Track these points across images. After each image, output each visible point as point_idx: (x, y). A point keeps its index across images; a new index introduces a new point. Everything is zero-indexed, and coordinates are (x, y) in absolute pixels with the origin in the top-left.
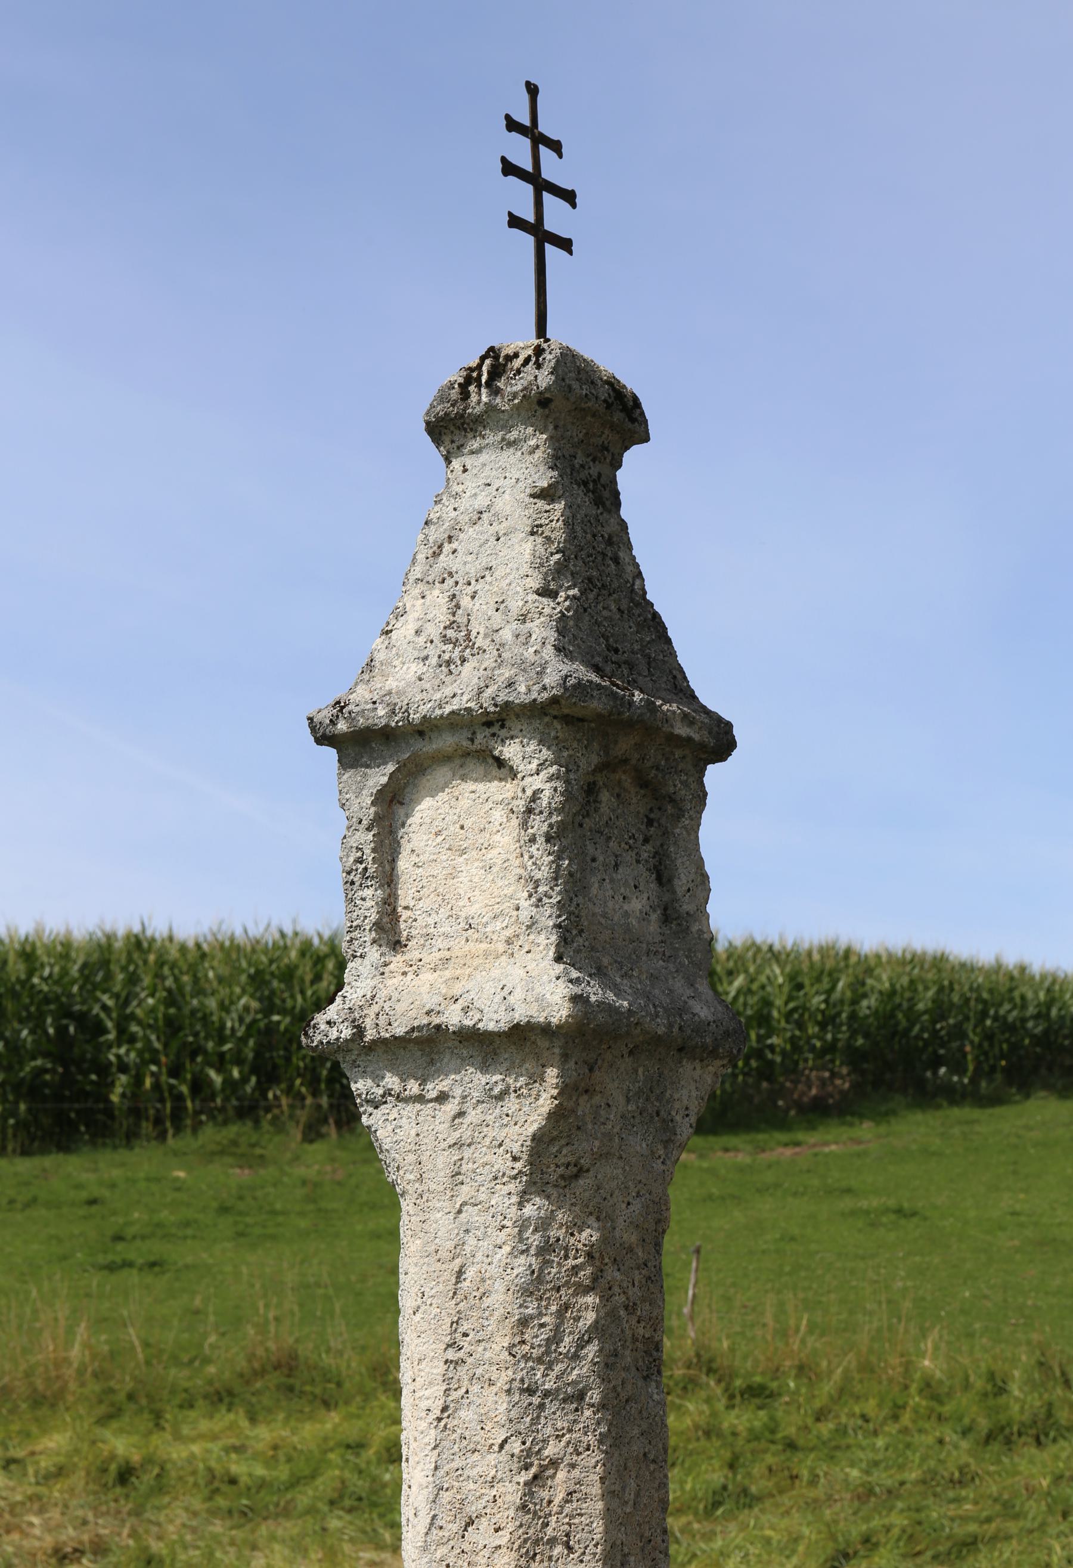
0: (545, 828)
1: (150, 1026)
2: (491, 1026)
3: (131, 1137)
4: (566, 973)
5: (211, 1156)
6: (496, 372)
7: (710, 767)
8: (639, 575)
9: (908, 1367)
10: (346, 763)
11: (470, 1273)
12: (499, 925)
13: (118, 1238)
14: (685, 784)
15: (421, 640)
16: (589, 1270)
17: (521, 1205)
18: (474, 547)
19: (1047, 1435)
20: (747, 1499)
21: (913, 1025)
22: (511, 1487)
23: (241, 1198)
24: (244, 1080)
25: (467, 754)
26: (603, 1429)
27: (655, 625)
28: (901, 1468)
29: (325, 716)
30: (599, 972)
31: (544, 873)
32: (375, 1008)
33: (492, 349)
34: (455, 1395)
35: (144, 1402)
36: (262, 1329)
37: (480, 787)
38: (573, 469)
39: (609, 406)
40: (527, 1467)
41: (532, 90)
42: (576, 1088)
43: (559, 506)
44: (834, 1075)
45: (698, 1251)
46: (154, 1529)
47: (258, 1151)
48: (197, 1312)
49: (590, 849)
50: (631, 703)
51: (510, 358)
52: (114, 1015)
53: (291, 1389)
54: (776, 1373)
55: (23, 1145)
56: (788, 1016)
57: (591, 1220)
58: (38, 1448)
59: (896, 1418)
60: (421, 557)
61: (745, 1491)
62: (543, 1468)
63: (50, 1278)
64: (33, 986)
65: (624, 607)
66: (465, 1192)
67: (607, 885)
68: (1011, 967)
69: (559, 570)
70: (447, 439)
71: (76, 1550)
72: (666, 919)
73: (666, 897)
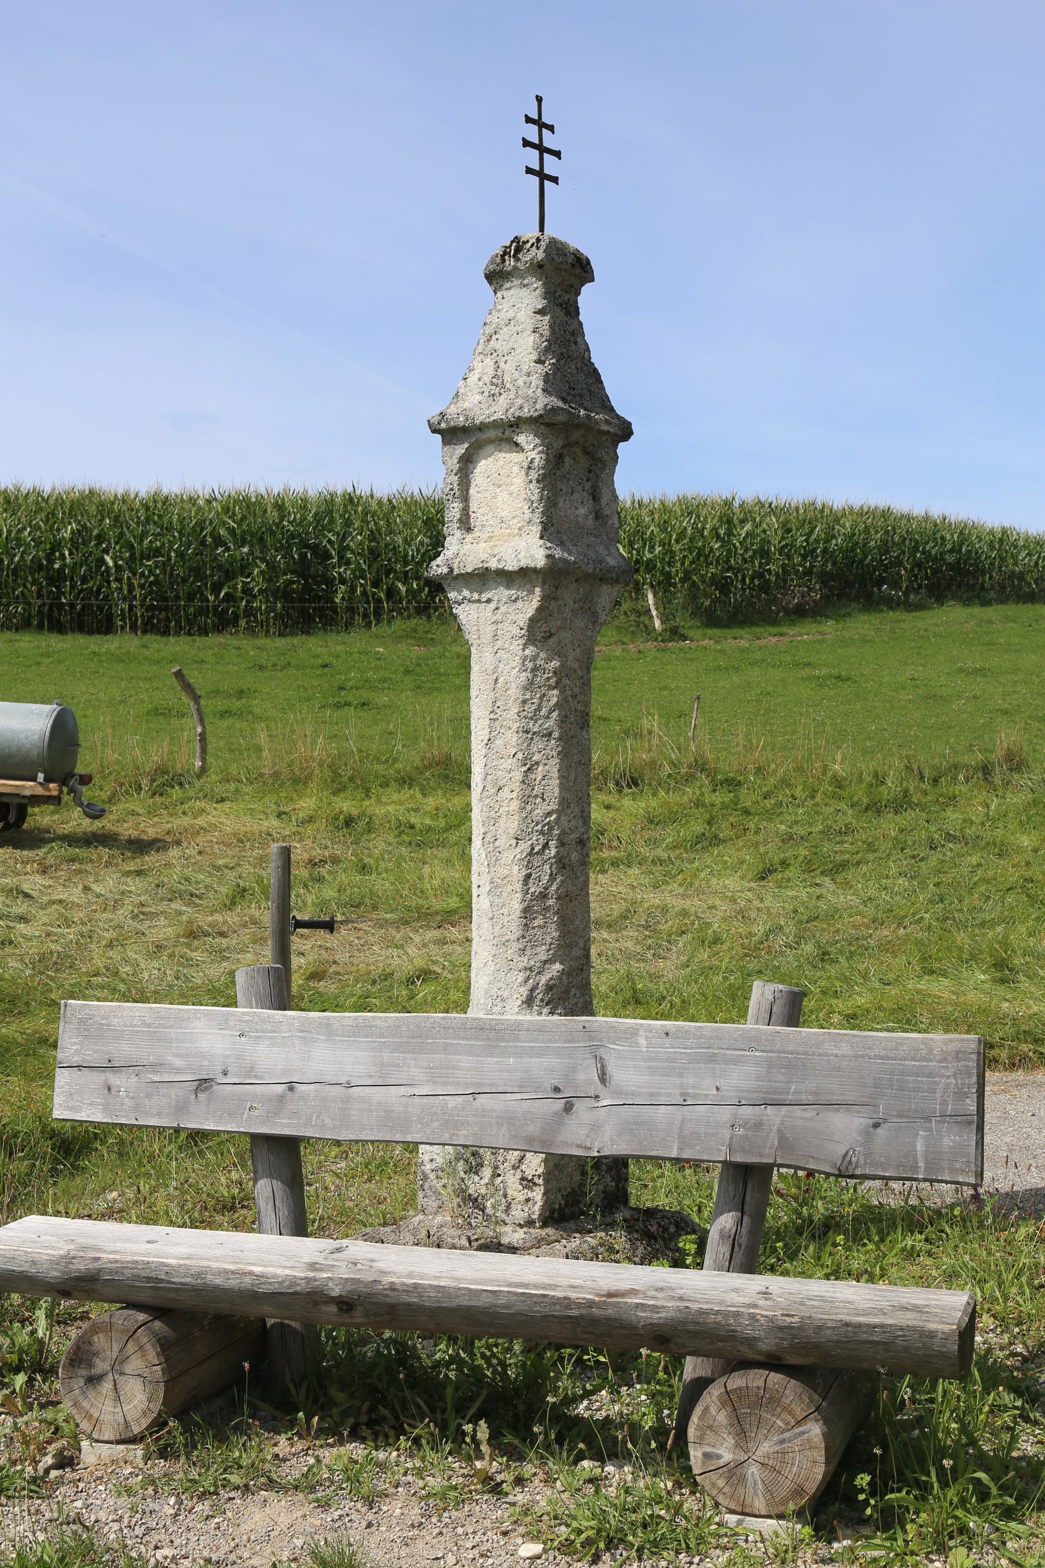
0: (536, 476)
1: (359, 554)
2: (510, 569)
3: (348, 625)
4: (545, 544)
5: (399, 638)
6: (518, 250)
7: (621, 444)
8: (588, 350)
9: (825, 769)
10: (445, 442)
11: (501, 680)
12: (515, 521)
13: (341, 688)
14: (608, 453)
15: (481, 383)
16: (554, 679)
17: (524, 650)
18: (506, 337)
19: (902, 807)
20: (716, 840)
21: (866, 557)
22: (518, 773)
23: (418, 665)
24: (421, 590)
25: (502, 440)
26: (560, 749)
27: (595, 374)
28: (811, 825)
29: (435, 420)
30: (561, 544)
31: (535, 497)
32: (459, 559)
33: (516, 237)
34: (494, 734)
35: (359, 782)
36: (430, 743)
37: (507, 455)
38: (555, 298)
39: (573, 266)
40: (525, 765)
41: (539, 100)
42: (549, 597)
43: (547, 318)
44: (810, 590)
45: (698, 698)
46: (367, 852)
47: (430, 636)
48: (391, 733)
49: (559, 485)
50: (579, 416)
51: (525, 243)
52: (336, 546)
53: (447, 777)
54: (744, 771)
55: (280, 630)
56: (781, 551)
57: (556, 657)
58: (297, 807)
59: (813, 797)
60: (481, 341)
61: (716, 837)
62: (533, 766)
63: (300, 711)
64: (284, 527)
65: (579, 366)
66: (499, 644)
67: (567, 502)
68: (936, 516)
69: (546, 350)
70: (495, 282)
71: (321, 861)
72: (597, 518)
73: (597, 507)
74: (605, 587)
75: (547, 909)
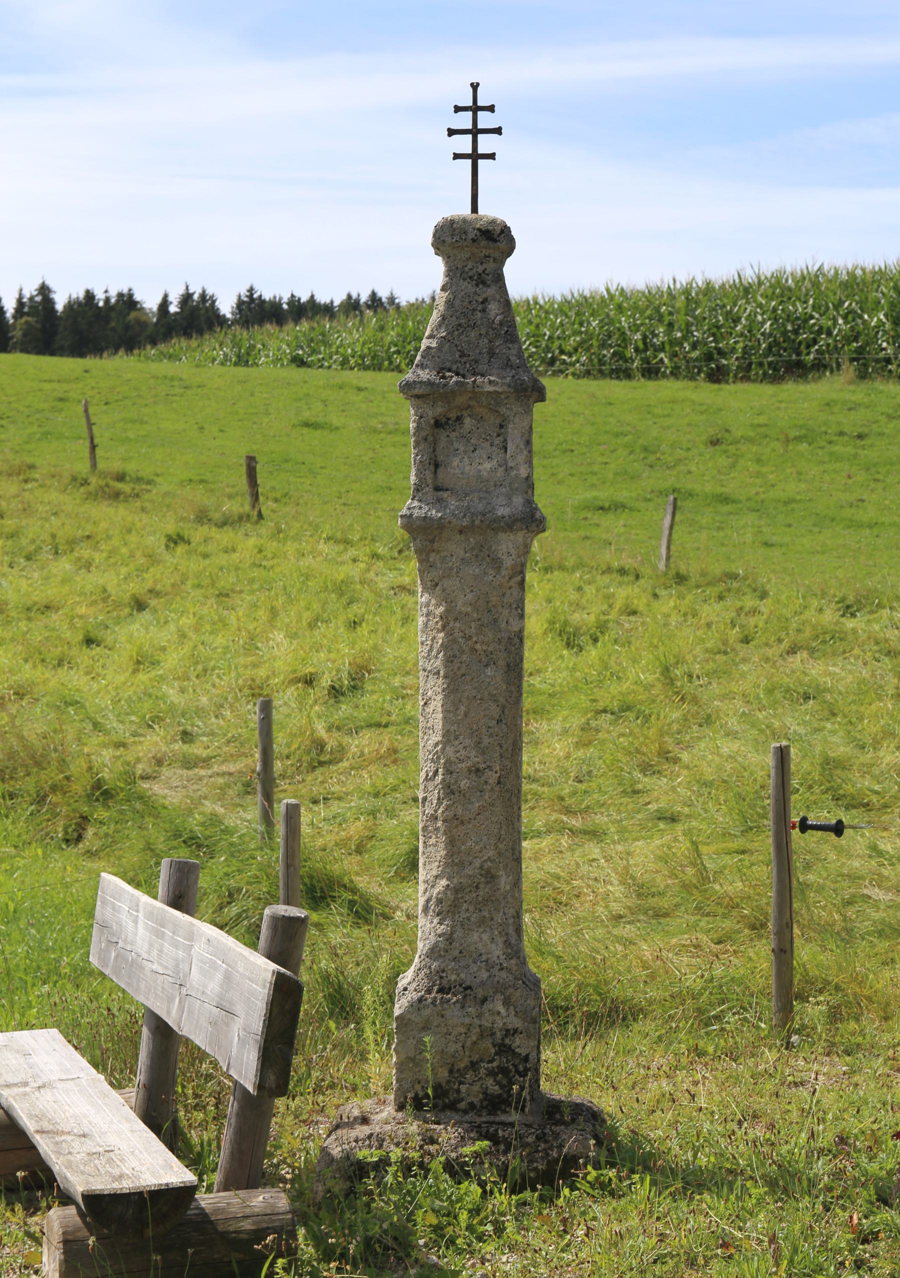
74: (502, 536)
75: (437, 829)
